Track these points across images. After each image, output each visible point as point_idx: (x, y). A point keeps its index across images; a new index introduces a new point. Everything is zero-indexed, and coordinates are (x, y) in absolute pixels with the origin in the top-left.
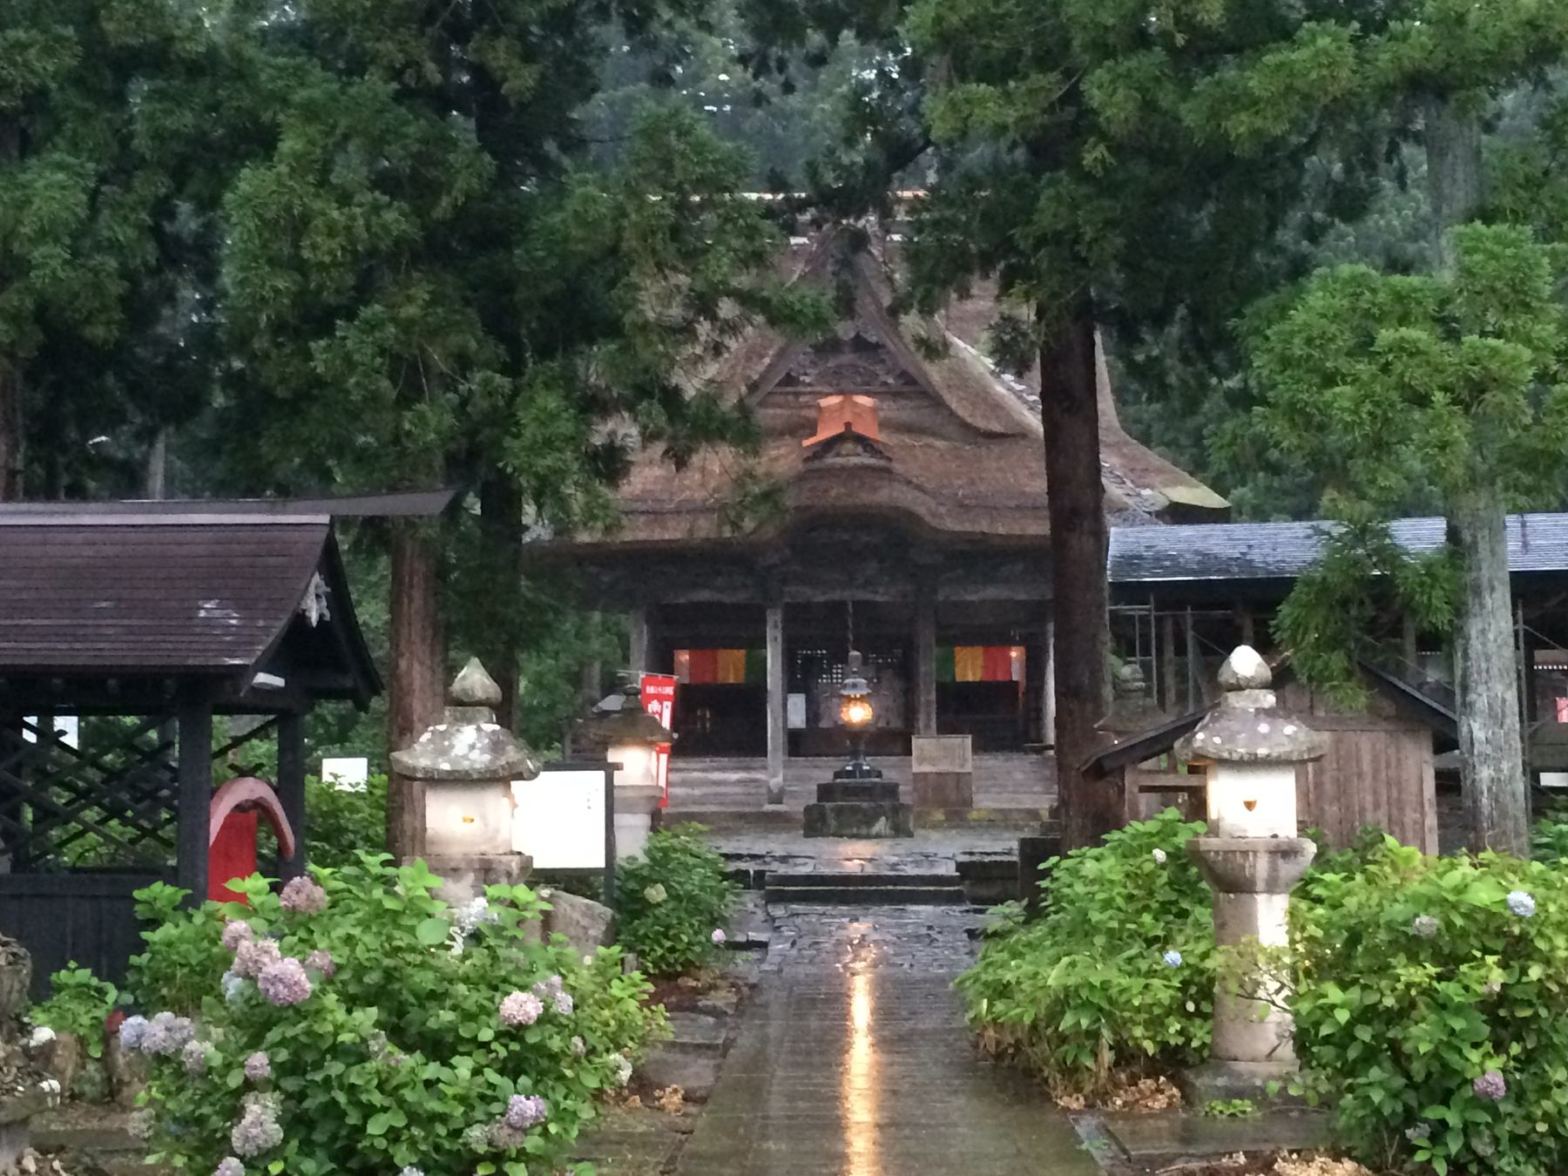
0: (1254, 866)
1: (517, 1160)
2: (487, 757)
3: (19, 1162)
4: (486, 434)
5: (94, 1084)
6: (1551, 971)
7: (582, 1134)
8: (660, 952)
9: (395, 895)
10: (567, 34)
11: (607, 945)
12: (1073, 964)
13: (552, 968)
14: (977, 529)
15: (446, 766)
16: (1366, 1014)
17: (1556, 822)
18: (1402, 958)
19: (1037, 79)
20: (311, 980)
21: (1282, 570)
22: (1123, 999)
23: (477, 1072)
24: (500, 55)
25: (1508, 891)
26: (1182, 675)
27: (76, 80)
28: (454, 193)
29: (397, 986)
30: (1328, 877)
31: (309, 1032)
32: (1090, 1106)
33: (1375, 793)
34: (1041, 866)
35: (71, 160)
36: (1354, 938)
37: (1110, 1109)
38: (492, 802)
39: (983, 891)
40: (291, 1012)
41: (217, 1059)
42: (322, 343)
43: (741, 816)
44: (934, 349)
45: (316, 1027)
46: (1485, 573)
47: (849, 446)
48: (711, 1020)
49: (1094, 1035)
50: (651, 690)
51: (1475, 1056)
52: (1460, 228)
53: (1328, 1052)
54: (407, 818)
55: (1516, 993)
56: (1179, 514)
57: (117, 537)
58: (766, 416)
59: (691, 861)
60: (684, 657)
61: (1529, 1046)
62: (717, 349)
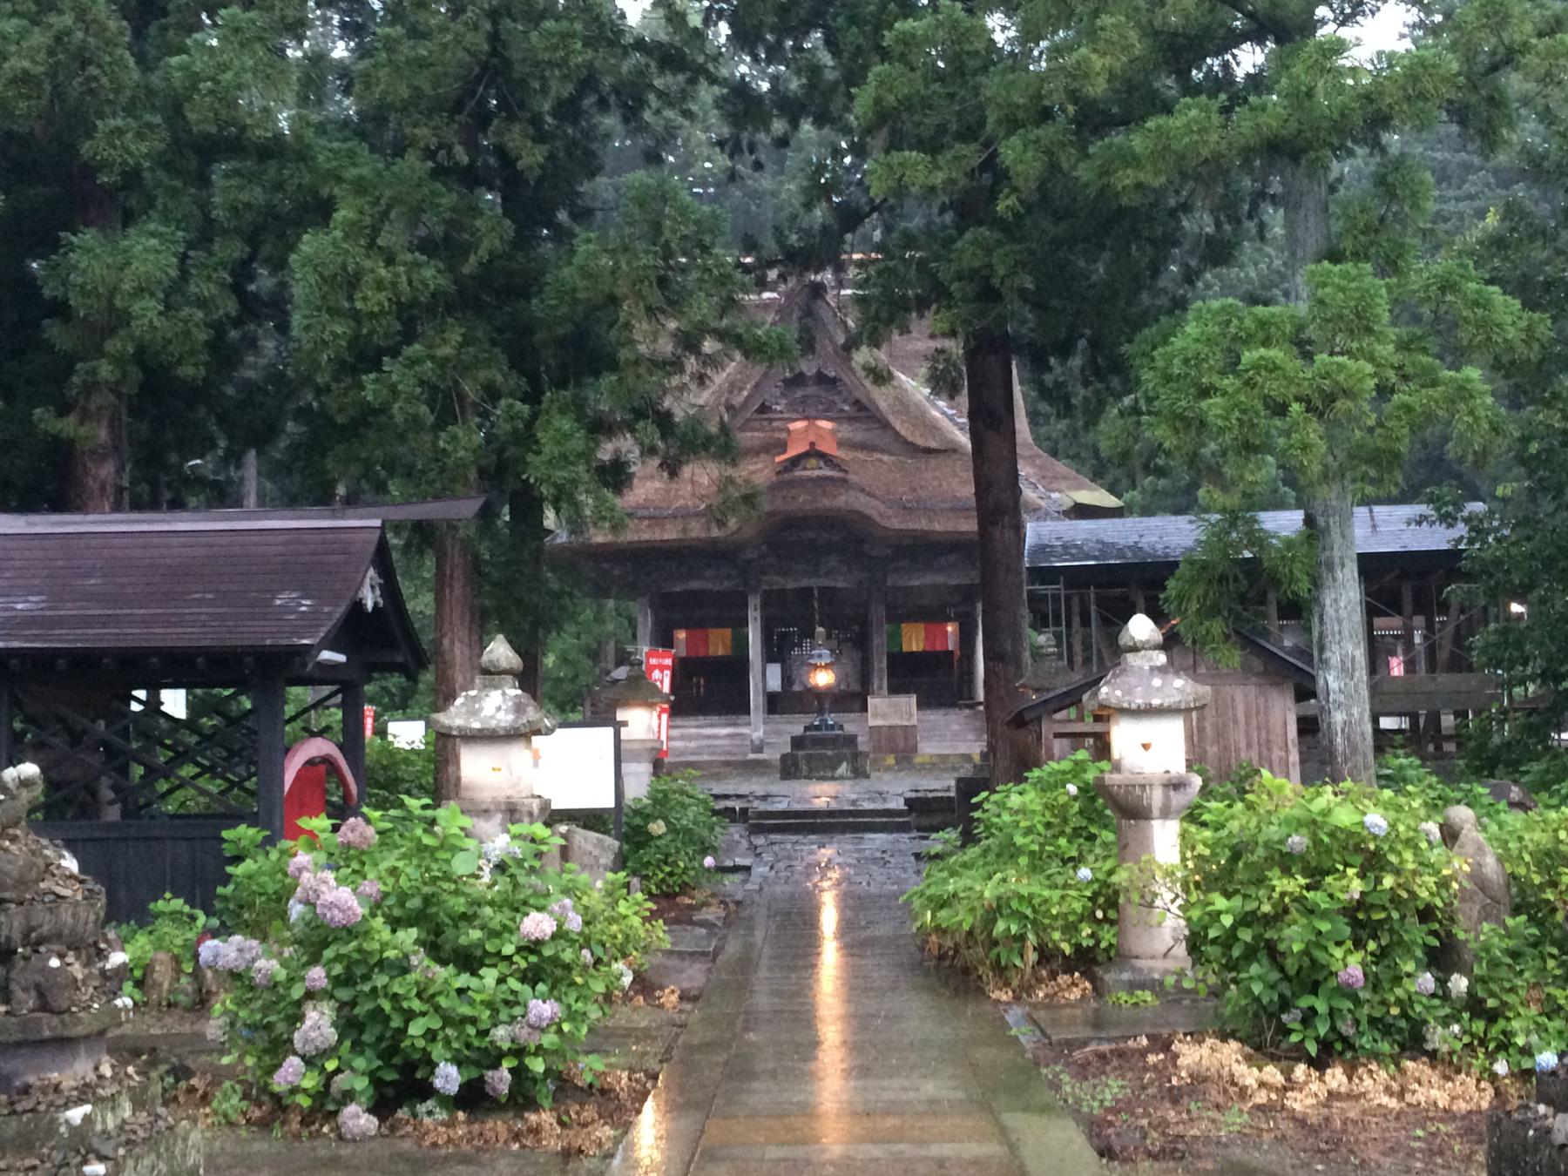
0: (1150, 798)
1: (536, 1054)
2: (511, 717)
3: (96, 1068)
4: (512, 451)
5: (187, 994)
6: (1402, 881)
7: (590, 1030)
8: (661, 876)
9: (434, 834)
10: (575, 123)
11: (615, 871)
12: (1004, 880)
13: (567, 891)
14: (917, 526)
15: (476, 725)
16: (1245, 920)
17: (1397, 757)
18: (1276, 872)
19: (961, 148)
20: (361, 904)
21: (1167, 555)
22: (1043, 908)
23: (501, 980)
24: (516, 138)
25: (1364, 814)
26: (1087, 646)
27: (166, 163)
28: (480, 252)
29: (434, 910)
30: (1213, 805)
31: (359, 950)
32: (1017, 998)
33: (1247, 734)
34: (974, 800)
35: (162, 229)
36: (1236, 855)
37: (1034, 1000)
38: (516, 754)
39: (925, 821)
40: (344, 934)
41: (282, 975)
42: (372, 376)
43: (727, 764)
44: (880, 377)
45: (365, 946)
46: (1336, 554)
47: (813, 462)
48: (703, 931)
49: (1021, 938)
50: (653, 661)
51: (1338, 953)
52: (1313, 267)
53: (1211, 950)
54: (451, 769)
55: (1370, 899)
56: (1082, 511)
57: (203, 540)
58: (746, 438)
59: (687, 800)
60: (681, 635)
61: (1383, 943)
62: (701, 379)
